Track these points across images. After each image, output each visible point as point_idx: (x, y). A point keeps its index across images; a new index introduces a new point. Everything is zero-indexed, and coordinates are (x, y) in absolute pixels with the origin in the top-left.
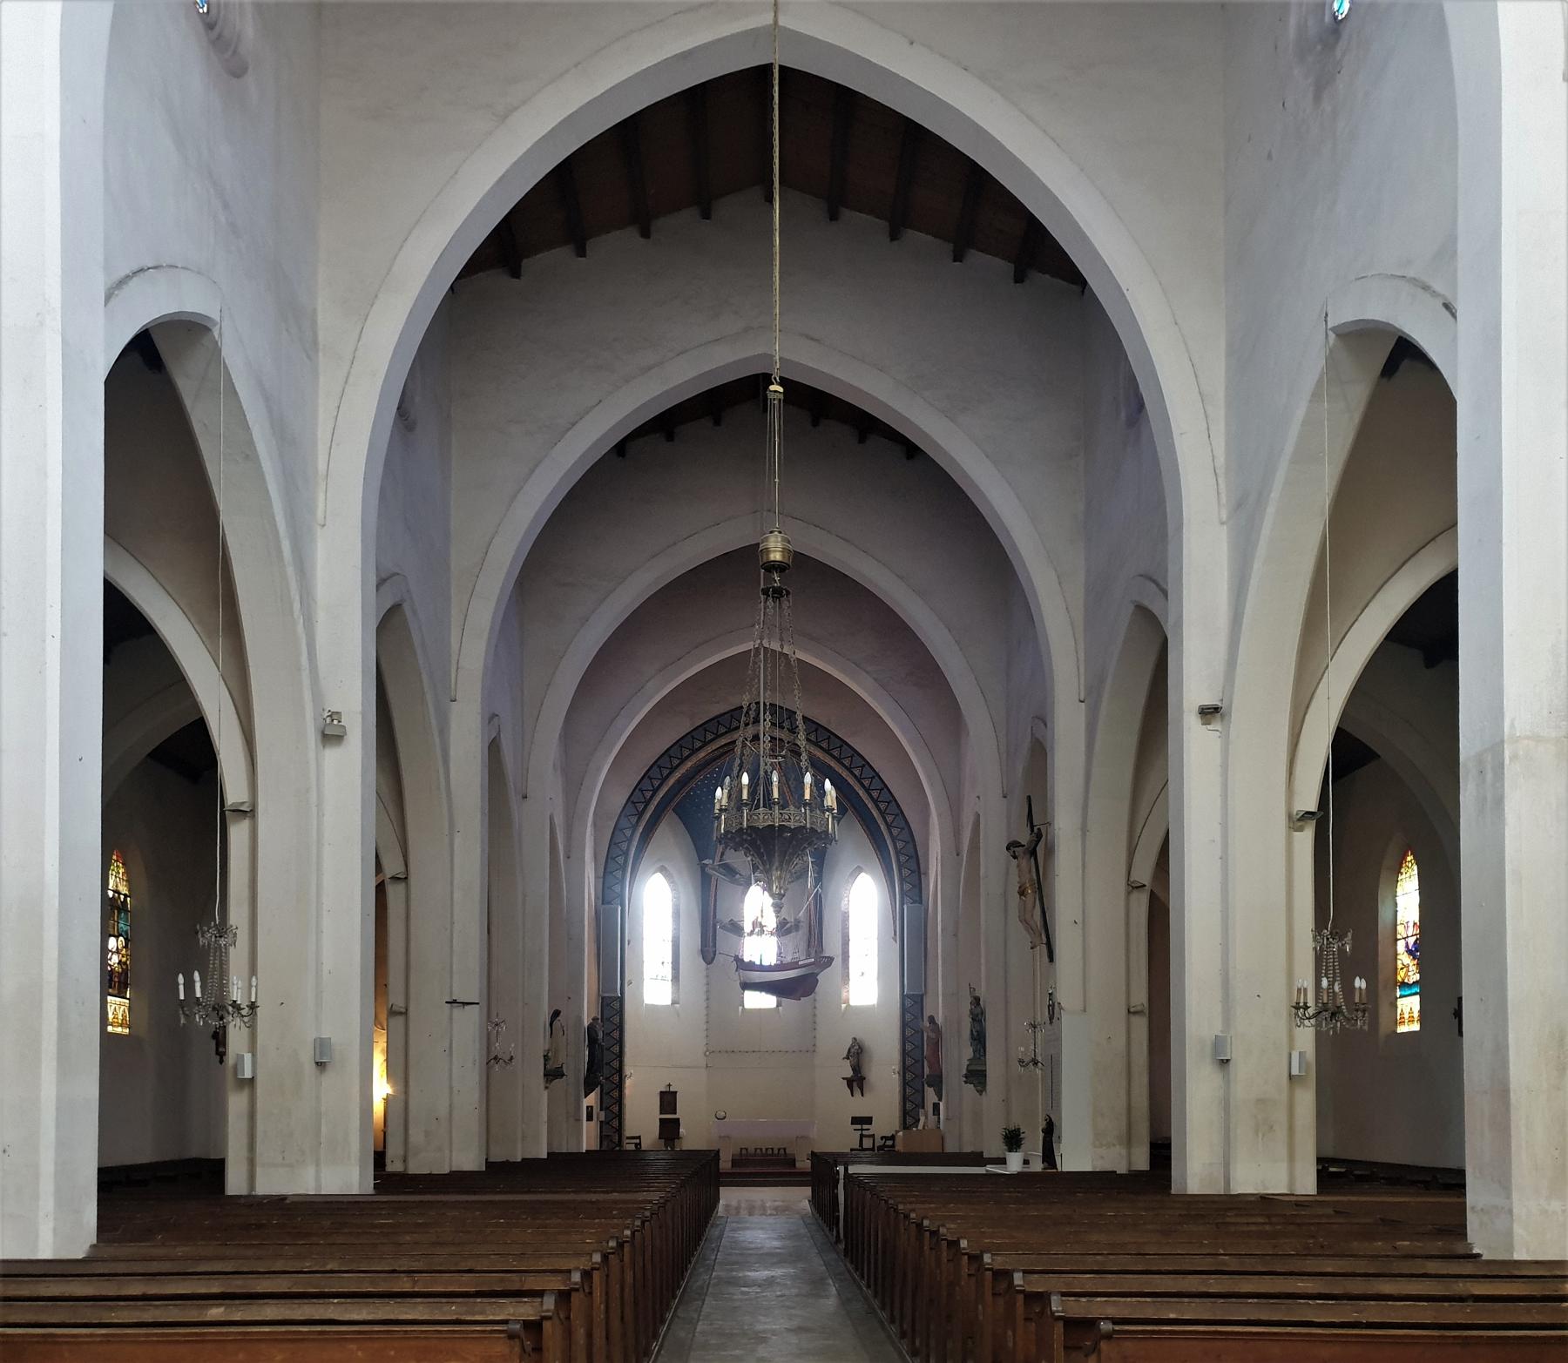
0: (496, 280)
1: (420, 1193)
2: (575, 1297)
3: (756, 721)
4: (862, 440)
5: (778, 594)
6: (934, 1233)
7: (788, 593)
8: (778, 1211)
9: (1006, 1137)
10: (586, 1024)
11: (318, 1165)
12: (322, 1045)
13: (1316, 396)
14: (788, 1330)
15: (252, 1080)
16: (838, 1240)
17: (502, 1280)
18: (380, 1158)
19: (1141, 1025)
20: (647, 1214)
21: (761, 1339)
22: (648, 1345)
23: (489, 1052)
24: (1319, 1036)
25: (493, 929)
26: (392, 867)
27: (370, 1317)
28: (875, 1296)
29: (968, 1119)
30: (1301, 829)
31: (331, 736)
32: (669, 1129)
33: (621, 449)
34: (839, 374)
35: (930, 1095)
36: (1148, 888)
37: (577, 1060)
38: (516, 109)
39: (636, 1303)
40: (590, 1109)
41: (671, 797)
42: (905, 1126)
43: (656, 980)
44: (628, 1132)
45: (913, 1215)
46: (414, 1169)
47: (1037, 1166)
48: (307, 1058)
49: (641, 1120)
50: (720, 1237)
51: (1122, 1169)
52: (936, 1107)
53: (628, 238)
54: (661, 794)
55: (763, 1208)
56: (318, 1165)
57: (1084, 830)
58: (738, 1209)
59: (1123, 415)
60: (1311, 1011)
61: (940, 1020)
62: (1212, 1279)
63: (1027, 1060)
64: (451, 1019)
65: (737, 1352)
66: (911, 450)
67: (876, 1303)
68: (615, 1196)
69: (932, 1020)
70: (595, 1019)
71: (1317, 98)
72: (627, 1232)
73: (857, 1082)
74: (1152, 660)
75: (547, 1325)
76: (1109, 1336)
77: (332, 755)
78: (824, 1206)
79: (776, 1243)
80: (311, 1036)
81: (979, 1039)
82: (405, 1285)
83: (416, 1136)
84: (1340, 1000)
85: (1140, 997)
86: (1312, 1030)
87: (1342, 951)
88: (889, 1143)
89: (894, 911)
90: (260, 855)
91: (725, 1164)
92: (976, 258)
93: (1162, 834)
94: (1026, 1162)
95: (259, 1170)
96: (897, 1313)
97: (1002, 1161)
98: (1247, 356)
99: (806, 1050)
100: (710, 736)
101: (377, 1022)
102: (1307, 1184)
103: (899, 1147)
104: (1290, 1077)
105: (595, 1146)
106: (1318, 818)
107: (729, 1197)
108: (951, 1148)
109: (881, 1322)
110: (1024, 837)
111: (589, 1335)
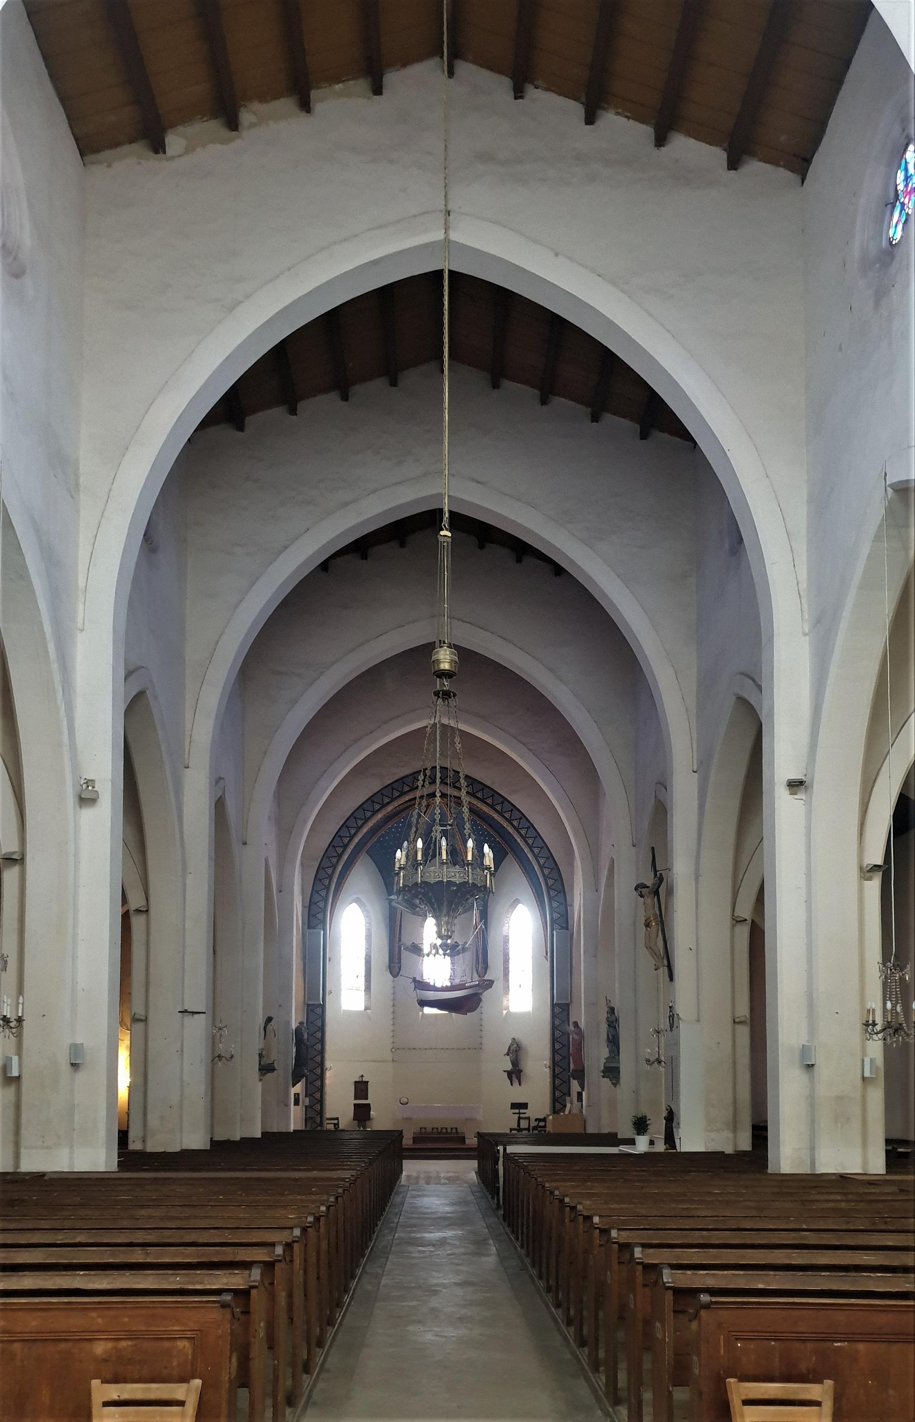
0: (224, 433)
1: (157, 1170)
2: (278, 1266)
3: (433, 782)
4: (519, 560)
5: (446, 695)
6: (573, 1208)
7: (455, 695)
8: (451, 1180)
9: (635, 1124)
10: (294, 1027)
11: (71, 1148)
12: (76, 1049)
13: (877, 538)
14: (456, 1284)
15: (18, 1078)
16: (498, 1207)
17: (218, 1253)
18: (123, 1136)
19: (744, 1033)
20: (340, 1190)
21: (433, 1291)
22: (340, 1298)
23: (213, 1050)
24: (887, 1049)
25: (218, 949)
26: (136, 901)
27: (109, 1287)
28: (528, 1256)
29: (606, 1106)
30: (870, 879)
31: (86, 799)
32: (362, 1113)
33: (324, 566)
34: (498, 510)
35: (575, 1085)
36: (749, 922)
37: (286, 1056)
38: (241, 302)
39: (330, 1266)
40: (297, 1096)
41: (365, 837)
42: (555, 1111)
43: (350, 990)
44: (329, 1114)
45: (557, 1193)
46: (150, 1149)
47: (660, 1147)
48: (63, 1060)
49: (339, 1104)
50: (402, 1203)
51: (729, 1150)
52: (580, 1095)
53: (331, 400)
54: (356, 840)
55: (438, 1178)
56: (71, 1148)
57: (697, 876)
58: (417, 1179)
59: (727, 546)
60: (879, 1028)
61: (582, 1025)
62: (794, 1253)
63: (652, 1059)
64: (183, 1025)
65: (414, 1303)
66: (558, 570)
67: (528, 1261)
68: (315, 1174)
69: (576, 1024)
70: (301, 1023)
71: (877, 304)
72: (323, 1208)
73: (515, 1074)
74: (748, 745)
75: (254, 1292)
76: (707, 1306)
77: (87, 814)
78: (487, 1177)
79: (447, 1209)
80: (67, 1042)
81: (614, 1041)
82: (138, 1256)
83: (153, 1121)
84: (901, 1019)
85: (743, 1011)
86: (880, 1043)
87: (902, 979)
88: (542, 1124)
89: (546, 936)
90: (27, 891)
91: (407, 1141)
92: (609, 419)
93: (757, 884)
94: (652, 1143)
95: (23, 1151)
96: (544, 1269)
97: (632, 1142)
98: (822, 502)
99: (473, 1049)
100: (396, 794)
101: (122, 1023)
102: (877, 1165)
103: (549, 1128)
104: (864, 1078)
105: (301, 1126)
106: (883, 869)
107: (411, 1168)
108: (591, 1130)
109: (531, 1277)
110: (649, 881)
111: (290, 1296)
